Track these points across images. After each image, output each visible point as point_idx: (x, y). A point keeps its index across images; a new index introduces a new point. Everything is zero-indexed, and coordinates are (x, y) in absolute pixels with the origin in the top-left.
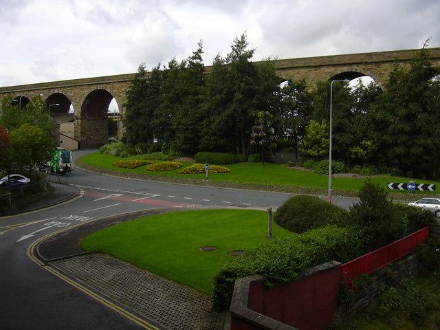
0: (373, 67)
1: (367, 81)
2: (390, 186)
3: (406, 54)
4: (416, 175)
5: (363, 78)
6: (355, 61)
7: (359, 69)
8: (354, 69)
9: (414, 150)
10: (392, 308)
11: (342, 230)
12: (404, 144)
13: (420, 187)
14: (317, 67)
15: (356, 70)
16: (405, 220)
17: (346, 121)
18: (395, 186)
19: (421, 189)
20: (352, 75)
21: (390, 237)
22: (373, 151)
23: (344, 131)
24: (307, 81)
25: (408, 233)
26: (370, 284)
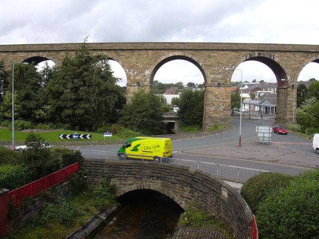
0: (54, 53)
1: (51, 64)
2: (61, 137)
3: (76, 45)
4: (82, 129)
5: (48, 61)
6: (41, 49)
7: (44, 55)
8: (41, 54)
9: (78, 111)
10: (50, 218)
11: (12, 168)
12: (72, 107)
13: (81, 137)
14: (14, 52)
15: (42, 55)
16: (60, 159)
17: (32, 92)
18: (64, 137)
19: (82, 138)
20: (38, 60)
21: (50, 170)
22: (51, 113)
23: (31, 99)
24: (5, 62)
25: (63, 166)
26: (34, 203)
